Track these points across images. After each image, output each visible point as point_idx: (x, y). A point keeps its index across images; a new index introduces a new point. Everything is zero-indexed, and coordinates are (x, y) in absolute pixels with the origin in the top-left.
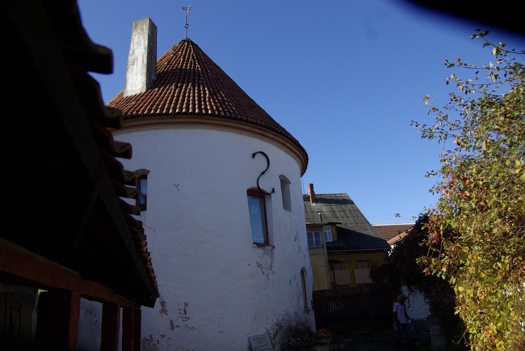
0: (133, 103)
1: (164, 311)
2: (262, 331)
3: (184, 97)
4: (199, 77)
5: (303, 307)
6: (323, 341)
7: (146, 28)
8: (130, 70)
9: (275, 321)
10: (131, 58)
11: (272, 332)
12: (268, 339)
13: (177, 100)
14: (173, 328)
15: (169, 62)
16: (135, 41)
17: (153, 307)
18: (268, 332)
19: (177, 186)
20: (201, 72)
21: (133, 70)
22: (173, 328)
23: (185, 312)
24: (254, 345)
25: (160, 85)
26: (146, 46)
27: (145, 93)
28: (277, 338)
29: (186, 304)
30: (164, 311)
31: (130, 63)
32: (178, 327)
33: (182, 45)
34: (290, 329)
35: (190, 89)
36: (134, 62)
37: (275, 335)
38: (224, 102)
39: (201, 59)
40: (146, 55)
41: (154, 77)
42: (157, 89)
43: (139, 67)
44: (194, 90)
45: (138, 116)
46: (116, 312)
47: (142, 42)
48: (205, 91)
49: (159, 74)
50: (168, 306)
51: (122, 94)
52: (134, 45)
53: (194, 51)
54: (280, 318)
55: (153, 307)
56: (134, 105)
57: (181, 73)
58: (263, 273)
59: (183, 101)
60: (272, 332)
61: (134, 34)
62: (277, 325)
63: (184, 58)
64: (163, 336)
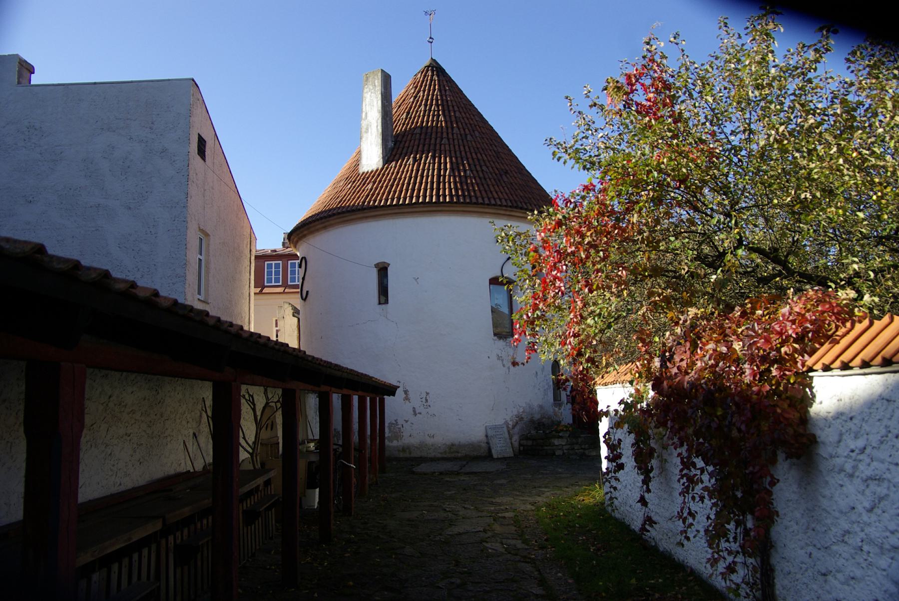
0: (370, 186)
1: (407, 399)
2: (500, 421)
3: (422, 176)
4: (442, 139)
5: (552, 400)
6: (560, 434)
7: (378, 82)
8: (364, 139)
9: (515, 413)
10: (364, 123)
11: (511, 423)
12: (505, 429)
13: (415, 183)
14: (415, 414)
15: (408, 113)
16: (368, 100)
17: (394, 395)
18: (506, 423)
19: (416, 279)
20: (444, 130)
21: (367, 138)
22: (415, 414)
23: (427, 401)
24: (490, 433)
25: (396, 158)
26: (380, 108)
27: (382, 169)
28: (517, 429)
29: (428, 394)
30: (407, 399)
31: (364, 130)
32: (826, 581)
33: (425, 76)
34: (532, 421)
35: (430, 163)
36: (367, 129)
37: (514, 427)
38: (466, 177)
39: (447, 101)
40: (380, 121)
41: (391, 144)
42: (393, 164)
43: (374, 136)
44: (434, 163)
45: (375, 207)
46: (366, 399)
47: (375, 100)
48: (446, 163)
49: (397, 136)
50: (411, 395)
51: (357, 163)
52: (366, 107)
53: (440, 90)
54: (521, 410)
55: (394, 395)
56: (371, 189)
57: (421, 134)
58: (504, 366)
59: (421, 183)
60: (511, 423)
61: (365, 90)
62: (517, 416)
63: (426, 105)
64: (407, 421)
